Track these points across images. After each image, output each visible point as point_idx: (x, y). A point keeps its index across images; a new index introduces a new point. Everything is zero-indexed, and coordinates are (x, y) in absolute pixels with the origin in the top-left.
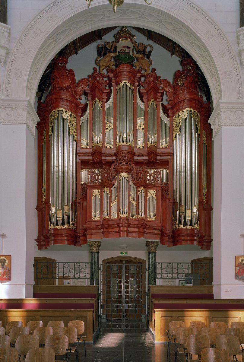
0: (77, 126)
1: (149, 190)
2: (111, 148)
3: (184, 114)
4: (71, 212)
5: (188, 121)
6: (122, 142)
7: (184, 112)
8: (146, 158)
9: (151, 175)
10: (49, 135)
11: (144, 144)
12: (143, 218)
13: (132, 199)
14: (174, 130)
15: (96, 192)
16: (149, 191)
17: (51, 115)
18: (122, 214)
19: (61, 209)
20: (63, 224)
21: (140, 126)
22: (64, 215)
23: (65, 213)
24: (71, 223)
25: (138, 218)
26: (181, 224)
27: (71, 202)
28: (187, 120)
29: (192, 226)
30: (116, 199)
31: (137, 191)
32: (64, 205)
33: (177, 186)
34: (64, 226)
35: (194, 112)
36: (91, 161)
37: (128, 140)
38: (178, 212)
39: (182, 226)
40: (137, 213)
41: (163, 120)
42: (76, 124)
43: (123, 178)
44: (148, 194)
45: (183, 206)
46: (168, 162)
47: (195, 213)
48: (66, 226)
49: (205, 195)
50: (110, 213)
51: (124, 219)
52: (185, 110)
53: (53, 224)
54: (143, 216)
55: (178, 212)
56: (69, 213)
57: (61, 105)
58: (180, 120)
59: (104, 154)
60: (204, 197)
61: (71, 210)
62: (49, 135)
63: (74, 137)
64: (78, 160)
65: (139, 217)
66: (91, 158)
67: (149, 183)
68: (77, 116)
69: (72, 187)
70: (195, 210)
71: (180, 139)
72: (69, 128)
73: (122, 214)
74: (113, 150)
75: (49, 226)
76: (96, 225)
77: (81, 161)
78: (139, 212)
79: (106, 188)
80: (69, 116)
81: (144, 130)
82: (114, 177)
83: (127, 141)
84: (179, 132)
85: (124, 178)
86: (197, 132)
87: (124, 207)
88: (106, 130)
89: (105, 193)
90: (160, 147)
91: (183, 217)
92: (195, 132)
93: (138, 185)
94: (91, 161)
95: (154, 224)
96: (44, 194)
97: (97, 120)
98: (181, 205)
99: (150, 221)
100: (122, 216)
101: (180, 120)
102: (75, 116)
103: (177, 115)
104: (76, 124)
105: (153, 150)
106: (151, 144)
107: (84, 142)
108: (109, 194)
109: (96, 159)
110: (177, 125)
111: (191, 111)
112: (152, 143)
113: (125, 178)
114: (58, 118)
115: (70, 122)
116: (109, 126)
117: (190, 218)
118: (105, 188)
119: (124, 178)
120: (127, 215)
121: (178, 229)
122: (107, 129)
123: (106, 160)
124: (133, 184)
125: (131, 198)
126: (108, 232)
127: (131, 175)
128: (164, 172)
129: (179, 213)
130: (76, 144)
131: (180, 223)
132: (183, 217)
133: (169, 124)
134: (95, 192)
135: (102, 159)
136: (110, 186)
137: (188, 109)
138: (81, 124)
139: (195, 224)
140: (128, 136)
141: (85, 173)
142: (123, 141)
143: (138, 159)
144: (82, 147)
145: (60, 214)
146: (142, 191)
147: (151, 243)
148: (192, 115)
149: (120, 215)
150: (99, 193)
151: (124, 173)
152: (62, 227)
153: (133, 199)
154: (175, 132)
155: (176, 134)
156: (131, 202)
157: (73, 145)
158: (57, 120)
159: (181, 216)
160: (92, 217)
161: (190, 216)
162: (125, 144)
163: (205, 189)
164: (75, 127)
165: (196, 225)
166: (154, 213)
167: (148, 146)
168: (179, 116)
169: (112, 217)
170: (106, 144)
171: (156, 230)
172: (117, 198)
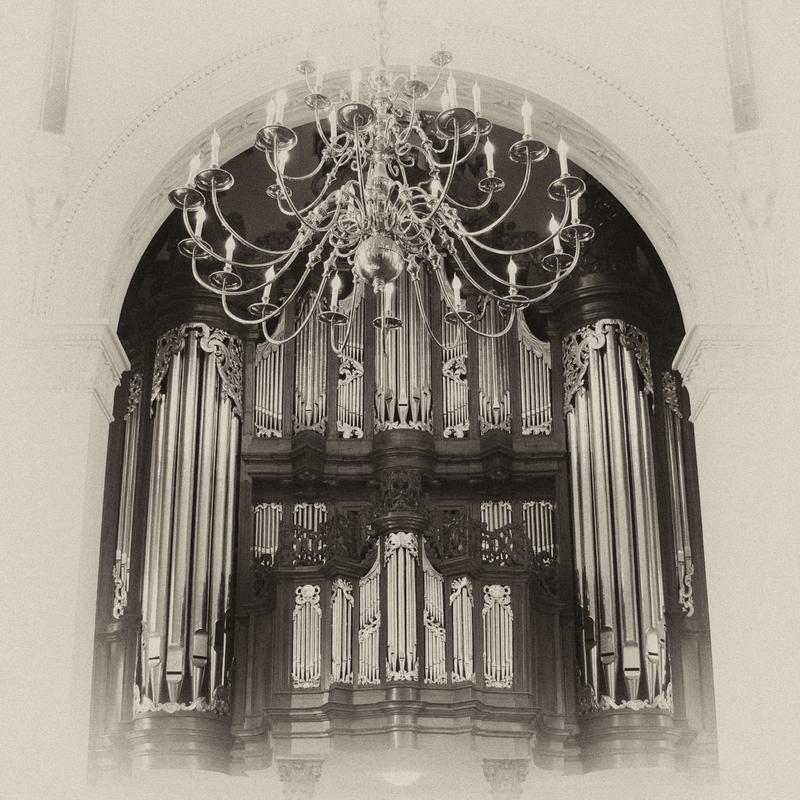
0: (243, 371)
1: (487, 587)
2: (355, 436)
3: (596, 336)
4: (214, 654)
5: (610, 351)
6: (395, 421)
7: (594, 329)
8: (475, 468)
9: (495, 534)
10: (152, 400)
11: (468, 423)
12: (470, 682)
13: (429, 618)
14: (568, 382)
15: (309, 590)
16: (487, 590)
17: (164, 342)
18: (398, 669)
19: (182, 646)
20: (185, 695)
21: (454, 368)
22: (191, 663)
23: (195, 657)
24: (213, 692)
25: (453, 681)
26: (608, 695)
27: (215, 620)
28: (606, 351)
29: (646, 701)
30: (375, 619)
31: (447, 591)
32: (192, 630)
33: (584, 561)
34: (188, 705)
35: (628, 328)
36: (289, 478)
37: (415, 416)
38: (594, 651)
39: (610, 701)
40: (450, 667)
41: (529, 349)
42: (240, 364)
43: (397, 550)
44: (486, 597)
45: (609, 629)
46: (551, 480)
47: (656, 655)
48: (196, 704)
49: (688, 584)
50: (354, 666)
51: (403, 685)
52: (599, 325)
53: (150, 696)
54: (469, 675)
55: (594, 651)
56: (208, 658)
57: (196, 313)
58: (585, 352)
59: (335, 456)
60: (687, 591)
61: (215, 649)
62: (152, 400)
63: (233, 404)
64: (246, 478)
65: (457, 678)
66: (287, 468)
67: (487, 562)
68: (245, 340)
69: (223, 565)
70: (653, 643)
71: (589, 407)
72: (221, 379)
73: (398, 669)
74: (363, 443)
75: (136, 702)
76: (306, 706)
77: (255, 481)
78: (456, 661)
79: (340, 583)
80: (219, 343)
81: (466, 381)
82: (371, 546)
83: (409, 418)
84: (584, 390)
85: (401, 551)
86: (643, 390)
87: (401, 643)
88: (340, 381)
89: (338, 599)
90: (524, 433)
91: (612, 669)
92: (635, 389)
93: (448, 575)
94: (289, 478)
95: (510, 702)
96: (119, 587)
97: (310, 352)
98: (604, 629)
99: (494, 691)
100: (398, 676)
101: (585, 352)
102: (240, 341)
103: (574, 337)
104: (240, 364)
105: (499, 447)
106: (492, 426)
107: (269, 403)
108: (352, 601)
109: (307, 473)
110: (575, 366)
111: (617, 326)
112: (496, 421)
113: (405, 549)
114: (185, 354)
115: (223, 363)
116: (350, 370)
117: (638, 673)
118: (340, 581)
119: (401, 551)
120: (415, 674)
121: (600, 709)
122: (343, 377)
123: (338, 475)
124: (434, 567)
125: (426, 614)
126: (347, 730)
127: (424, 540)
128: (537, 513)
129: (600, 655)
130: (240, 425)
131: (603, 689)
132: (612, 669)
133: (548, 359)
134: (302, 592)
135: (325, 474)
136: (355, 576)
137: (608, 321)
138: (257, 364)
139: (657, 693)
140: (413, 400)
141: (269, 516)
142: (397, 418)
143: (449, 471)
144: (258, 435)
145: (176, 662)
146: (465, 590)
147: (500, 766)
148: (622, 339)
149: (390, 674)
150: (318, 598)
151: (401, 534)
152: (183, 706)
153: (433, 619)
154: (570, 387)
155: (574, 396)
156: (428, 626)
157: (228, 425)
158: (182, 358)
159: (606, 665)
160: (291, 678)
161: (639, 666)
162: (404, 425)
163: (689, 562)
164: (239, 374)
165: (661, 697)
166: (509, 662)
167: (483, 431)
168: (580, 339)
169: (363, 678)
170: (339, 423)
171: (515, 721)
172: (378, 616)
